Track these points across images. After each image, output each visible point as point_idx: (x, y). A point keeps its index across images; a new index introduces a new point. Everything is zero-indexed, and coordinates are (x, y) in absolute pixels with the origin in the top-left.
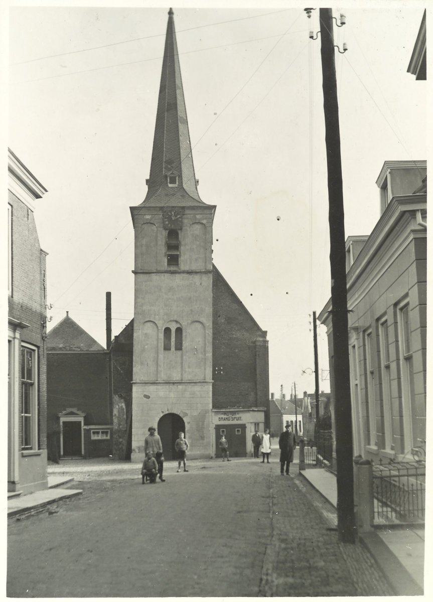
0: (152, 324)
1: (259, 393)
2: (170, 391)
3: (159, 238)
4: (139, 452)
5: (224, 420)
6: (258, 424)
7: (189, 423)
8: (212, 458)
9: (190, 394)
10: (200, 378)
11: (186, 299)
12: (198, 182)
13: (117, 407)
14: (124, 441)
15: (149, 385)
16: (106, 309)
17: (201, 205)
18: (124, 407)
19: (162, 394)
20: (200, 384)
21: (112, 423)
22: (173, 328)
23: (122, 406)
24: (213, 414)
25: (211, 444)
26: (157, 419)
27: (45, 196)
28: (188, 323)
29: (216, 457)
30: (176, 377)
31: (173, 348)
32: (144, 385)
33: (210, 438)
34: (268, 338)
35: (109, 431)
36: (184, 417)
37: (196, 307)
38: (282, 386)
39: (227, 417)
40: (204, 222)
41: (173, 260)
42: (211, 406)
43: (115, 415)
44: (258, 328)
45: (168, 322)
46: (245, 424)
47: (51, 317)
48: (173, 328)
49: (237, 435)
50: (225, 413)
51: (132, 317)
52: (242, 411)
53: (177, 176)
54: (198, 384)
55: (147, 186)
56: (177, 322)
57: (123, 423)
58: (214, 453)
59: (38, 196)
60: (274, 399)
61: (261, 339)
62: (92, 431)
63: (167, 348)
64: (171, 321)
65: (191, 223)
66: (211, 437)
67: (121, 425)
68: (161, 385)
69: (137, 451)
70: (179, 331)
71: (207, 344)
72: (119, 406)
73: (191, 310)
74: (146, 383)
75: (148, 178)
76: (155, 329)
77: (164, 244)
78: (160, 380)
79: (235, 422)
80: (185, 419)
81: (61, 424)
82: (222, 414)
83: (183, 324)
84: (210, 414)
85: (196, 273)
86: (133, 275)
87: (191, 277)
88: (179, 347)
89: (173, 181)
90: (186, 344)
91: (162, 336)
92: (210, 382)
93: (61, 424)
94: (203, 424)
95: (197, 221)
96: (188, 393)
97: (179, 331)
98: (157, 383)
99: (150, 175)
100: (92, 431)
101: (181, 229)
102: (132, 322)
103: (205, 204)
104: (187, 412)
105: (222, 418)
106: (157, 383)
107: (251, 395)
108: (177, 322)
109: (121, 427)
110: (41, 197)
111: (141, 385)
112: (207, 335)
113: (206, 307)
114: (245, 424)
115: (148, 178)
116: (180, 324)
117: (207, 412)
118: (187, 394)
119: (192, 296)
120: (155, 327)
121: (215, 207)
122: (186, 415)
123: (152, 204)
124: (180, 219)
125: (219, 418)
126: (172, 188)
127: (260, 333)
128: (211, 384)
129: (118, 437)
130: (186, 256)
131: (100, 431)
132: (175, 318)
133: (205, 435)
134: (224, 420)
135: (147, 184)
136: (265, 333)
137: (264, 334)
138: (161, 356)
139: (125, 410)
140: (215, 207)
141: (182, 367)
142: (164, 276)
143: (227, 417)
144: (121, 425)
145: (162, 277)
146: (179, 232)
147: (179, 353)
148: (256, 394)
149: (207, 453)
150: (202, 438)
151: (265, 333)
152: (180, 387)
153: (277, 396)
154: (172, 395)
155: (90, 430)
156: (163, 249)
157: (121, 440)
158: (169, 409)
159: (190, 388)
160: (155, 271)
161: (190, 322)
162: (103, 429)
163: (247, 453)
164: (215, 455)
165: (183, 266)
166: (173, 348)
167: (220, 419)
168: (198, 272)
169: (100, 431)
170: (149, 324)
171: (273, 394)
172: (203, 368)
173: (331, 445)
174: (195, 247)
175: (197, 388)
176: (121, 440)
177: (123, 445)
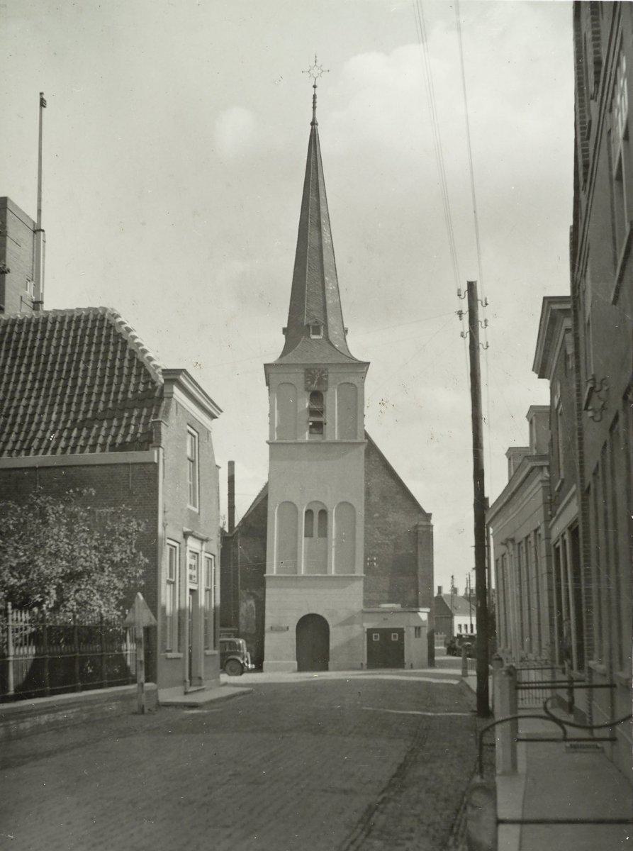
6: (419, 628)
11: (340, 484)
12: (347, 331)
16: (234, 494)
17: (354, 362)
21: (238, 626)
27: (221, 416)
34: (433, 522)
38: (452, 577)
43: (242, 615)
47: (486, 321)
49: (394, 641)
51: (266, 479)
53: (320, 326)
55: (284, 336)
59: (213, 417)
60: (442, 595)
61: (424, 523)
75: (286, 326)
81: (322, 334)
86: (268, 446)
89: (317, 332)
93: (322, 334)
99: (288, 324)
102: (266, 487)
103: (356, 360)
109: (249, 629)
110: (216, 417)
115: (286, 326)
121: (368, 363)
123: (291, 359)
124: (325, 379)
126: (314, 339)
128: (363, 579)
135: (284, 334)
136: (429, 516)
140: (368, 363)
151: (429, 516)
153: (447, 591)
171: (440, 588)
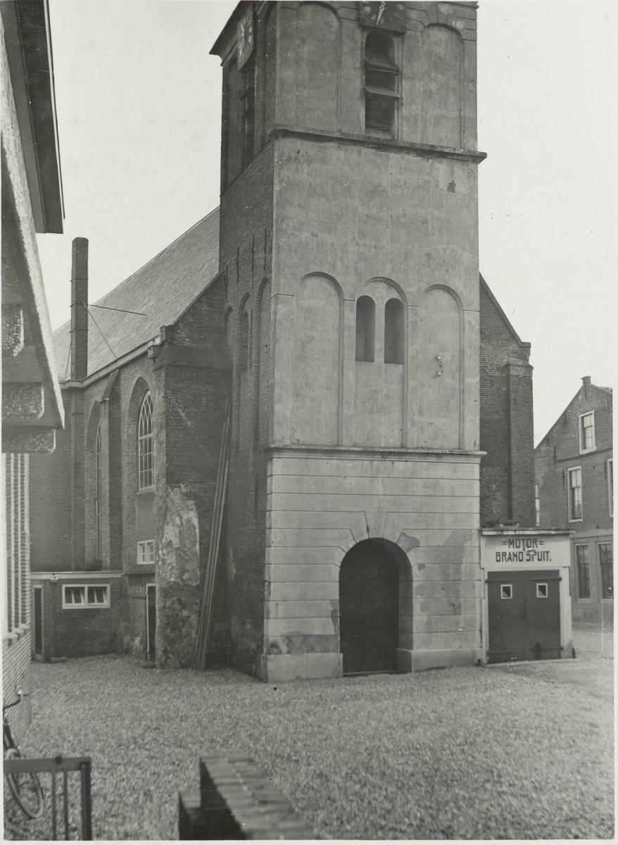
0: (325, 282)
1: (516, 495)
2: (374, 477)
3: (345, 49)
4: (288, 652)
5: (510, 558)
7: (421, 567)
8: (479, 663)
9: (425, 487)
10: (450, 443)
13: (177, 521)
14: (193, 617)
15: (319, 455)
18: (195, 522)
19: (351, 483)
20: (450, 459)
22: (381, 296)
23: (189, 521)
24: (483, 542)
25: (478, 623)
26: (340, 556)
28: (419, 290)
29: (489, 662)
30: (388, 436)
31: (379, 356)
32: (304, 455)
33: (473, 607)
34: (532, 361)
35: (108, 586)
36: (408, 551)
37: (440, 247)
39: (516, 550)
40: (459, 25)
41: (381, 112)
42: (476, 524)
44: (513, 336)
45: (367, 283)
46: (557, 572)
48: (381, 296)
50: (511, 541)
52: (555, 535)
54: (445, 459)
56: (391, 283)
57: (193, 565)
58: (485, 648)
62: (64, 586)
63: (365, 355)
64: (377, 280)
65: (427, 23)
66: (478, 605)
67: (187, 571)
68: (354, 457)
69: (284, 647)
70: (394, 308)
71: (468, 350)
72: (181, 518)
73: (428, 255)
74: (310, 451)
76: (335, 298)
77: (358, 65)
78: (346, 444)
79: (535, 565)
80: (412, 557)
82: (504, 543)
83: (407, 290)
84: (475, 541)
85: (442, 155)
87: (427, 164)
88: (395, 354)
90: (413, 347)
91: (351, 317)
92: (476, 456)
94: (458, 571)
95: (441, 21)
96: (420, 483)
97: (394, 308)
98: (339, 452)
100: (64, 586)
101: (401, 34)
104: (417, 535)
105: (504, 554)
106: (339, 452)
107: (495, 499)
108: (391, 283)
109: (186, 576)
111: (296, 455)
112: (467, 327)
113: (464, 250)
114: (557, 572)
116: (400, 291)
117: (466, 535)
118: (418, 487)
119: (430, 217)
120: (332, 290)
122: (415, 544)
125: (498, 554)
127: (514, 347)
128: (478, 460)
129: (177, 606)
130: (414, 107)
131: (86, 586)
132: (387, 272)
133: (462, 600)
134: (510, 558)
137: (526, 347)
138: (350, 375)
139: (197, 531)
141: (403, 411)
142: (359, 152)
143: (516, 550)
144: (187, 571)
145: (354, 156)
146: (396, 40)
147: (397, 370)
148: (509, 497)
149: (466, 650)
150: (456, 609)
152: (400, 465)
154: (379, 487)
155: (55, 585)
156: (355, 80)
157: (185, 613)
158: (371, 524)
159: (426, 469)
160: (337, 135)
161: (424, 286)
162: (92, 581)
163: (562, 649)
164: (488, 654)
165: (405, 131)
166: (379, 356)
167: (500, 557)
168: (448, 154)
169: (86, 586)
170: (315, 282)
172: (455, 415)
173: (149, 601)
174: (433, 86)
175: (442, 470)
176: (185, 613)
177: (191, 627)
